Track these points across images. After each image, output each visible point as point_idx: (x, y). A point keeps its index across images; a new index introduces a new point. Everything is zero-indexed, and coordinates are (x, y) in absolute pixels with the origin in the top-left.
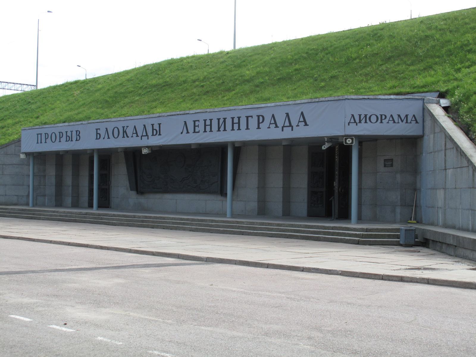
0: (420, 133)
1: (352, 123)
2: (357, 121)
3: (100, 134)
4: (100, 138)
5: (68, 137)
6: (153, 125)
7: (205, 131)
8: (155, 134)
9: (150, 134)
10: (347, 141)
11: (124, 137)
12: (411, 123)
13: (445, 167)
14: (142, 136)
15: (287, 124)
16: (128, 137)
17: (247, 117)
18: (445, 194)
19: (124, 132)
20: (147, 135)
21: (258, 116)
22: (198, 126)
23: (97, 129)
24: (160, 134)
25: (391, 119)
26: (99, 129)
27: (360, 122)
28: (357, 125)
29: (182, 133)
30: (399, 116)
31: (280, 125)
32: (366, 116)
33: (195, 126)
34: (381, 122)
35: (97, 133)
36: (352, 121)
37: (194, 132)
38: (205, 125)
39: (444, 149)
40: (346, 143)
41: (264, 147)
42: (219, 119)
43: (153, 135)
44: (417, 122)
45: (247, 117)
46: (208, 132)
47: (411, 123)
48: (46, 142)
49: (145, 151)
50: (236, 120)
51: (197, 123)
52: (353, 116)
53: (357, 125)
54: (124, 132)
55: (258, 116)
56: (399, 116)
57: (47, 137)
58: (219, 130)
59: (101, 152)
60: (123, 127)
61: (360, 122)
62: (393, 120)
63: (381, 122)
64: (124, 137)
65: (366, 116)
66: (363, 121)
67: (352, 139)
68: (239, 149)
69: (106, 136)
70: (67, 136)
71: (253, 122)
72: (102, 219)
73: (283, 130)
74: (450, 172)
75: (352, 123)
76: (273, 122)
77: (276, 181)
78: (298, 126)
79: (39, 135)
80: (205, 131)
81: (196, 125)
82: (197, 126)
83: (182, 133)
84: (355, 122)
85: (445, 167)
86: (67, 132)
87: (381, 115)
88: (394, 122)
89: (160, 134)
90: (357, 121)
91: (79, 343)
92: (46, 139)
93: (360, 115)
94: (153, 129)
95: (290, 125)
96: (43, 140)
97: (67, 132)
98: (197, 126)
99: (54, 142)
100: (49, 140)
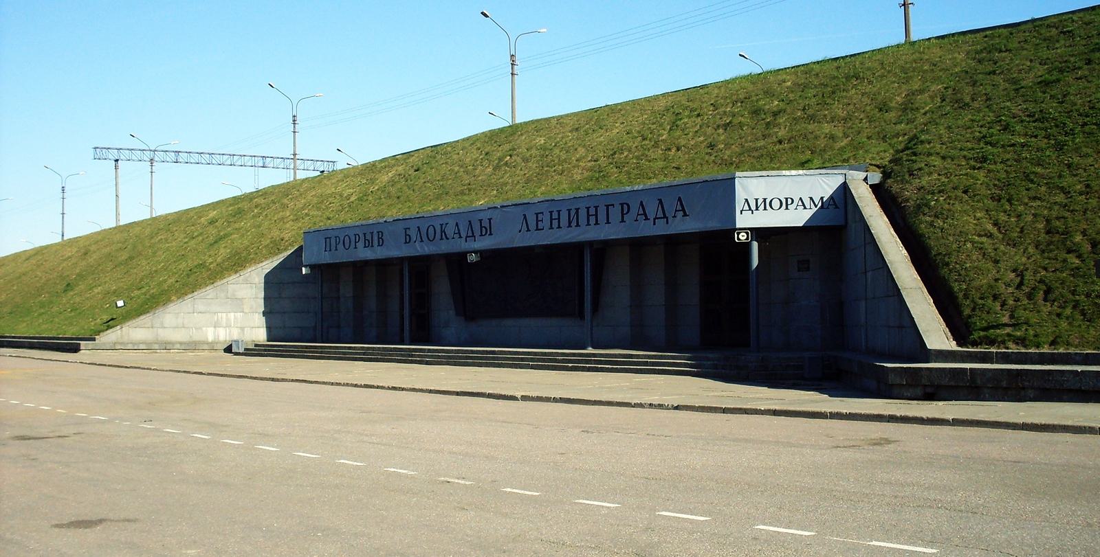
0: (840, 222)
1: (659, 218)
2: (753, 208)
3: (409, 236)
4: (410, 241)
5: (483, 229)
6: (481, 221)
7: (551, 228)
8: (367, 245)
9: (477, 233)
10: (740, 237)
11: (442, 239)
12: (828, 208)
13: (865, 269)
14: (655, 219)
15: (660, 214)
16: (447, 239)
17: (607, 206)
18: (866, 303)
19: (443, 231)
20: (473, 236)
21: (622, 205)
22: (542, 221)
23: (406, 229)
24: (491, 234)
25: (800, 203)
26: (409, 229)
27: (757, 209)
28: (752, 213)
29: (520, 231)
30: (811, 198)
31: (651, 216)
32: (765, 200)
33: (537, 221)
34: (787, 208)
35: (406, 235)
36: (746, 207)
37: (537, 229)
38: (551, 219)
39: (863, 243)
40: (738, 239)
41: (638, 246)
42: (569, 211)
43: (481, 235)
44: (837, 207)
45: (607, 206)
46: (555, 229)
47: (828, 208)
48: (336, 250)
49: (473, 258)
50: (592, 211)
51: (540, 217)
52: (747, 200)
53: (752, 213)
54: (443, 231)
55: (622, 205)
56: (811, 198)
57: (357, 241)
58: (570, 226)
59: (412, 260)
60: (442, 225)
61: (757, 209)
62: (804, 205)
63: (787, 208)
64: (442, 239)
65: (765, 200)
66: (762, 207)
67: (747, 233)
68: (602, 249)
69: (419, 239)
70: (365, 240)
71: (615, 213)
72: (412, 356)
73: (654, 224)
74: (869, 274)
75: (659, 218)
76: (641, 212)
77: (656, 295)
78: (675, 217)
79: (328, 240)
80: (551, 228)
81: (594, 217)
82: (540, 221)
83: (520, 231)
84: (750, 209)
85: (865, 269)
86: (365, 234)
87: (787, 199)
88: (805, 208)
89: (491, 234)
90: (753, 208)
91: (755, 428)
92: (356, 242)
93: (757, 200)
94: (481, 227)
95: (665, 217)
96: (333, 248)
97: (365, 234)
98: (540, 221)
99: (433, 239)
100: (340, 246)
